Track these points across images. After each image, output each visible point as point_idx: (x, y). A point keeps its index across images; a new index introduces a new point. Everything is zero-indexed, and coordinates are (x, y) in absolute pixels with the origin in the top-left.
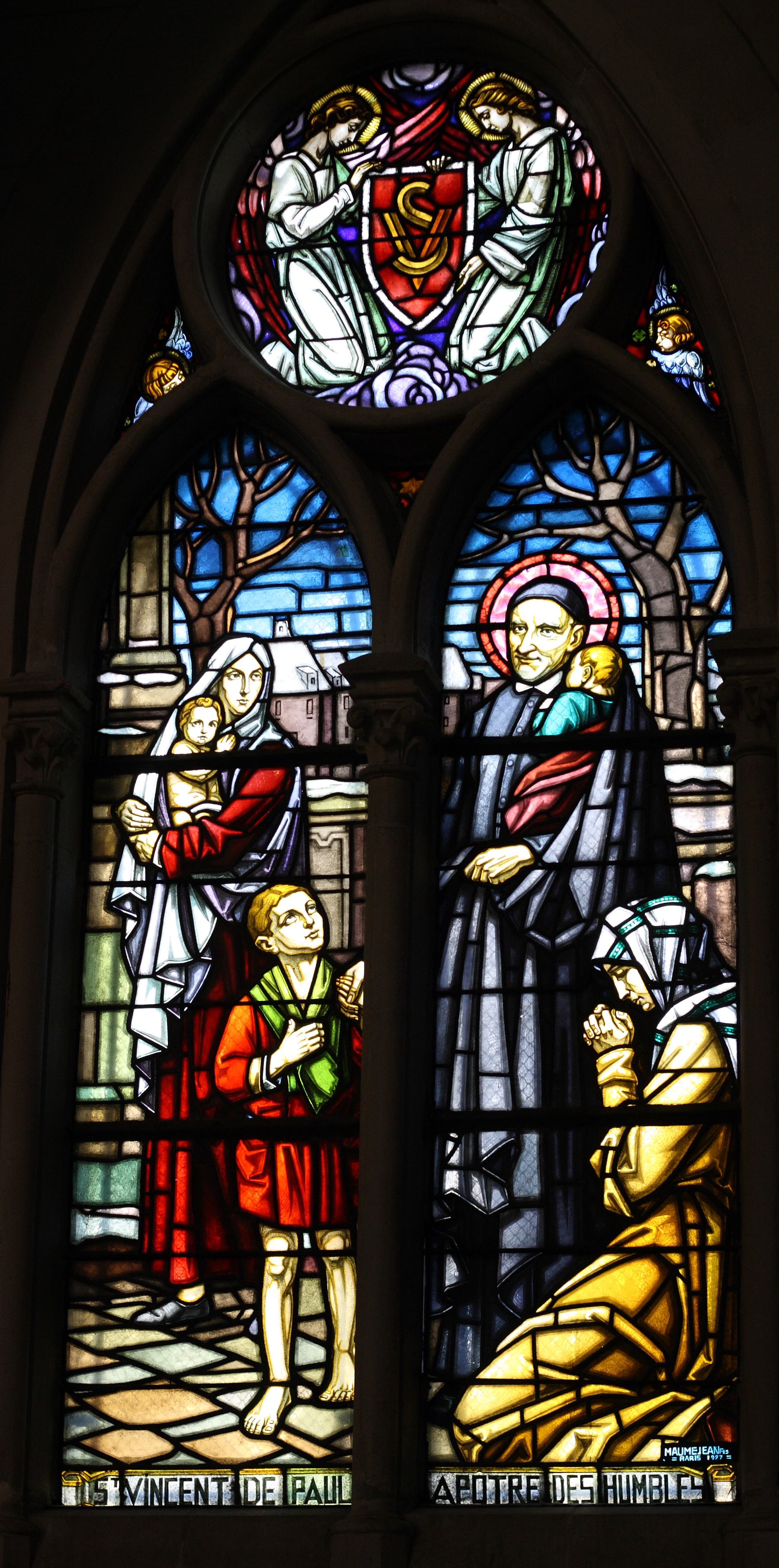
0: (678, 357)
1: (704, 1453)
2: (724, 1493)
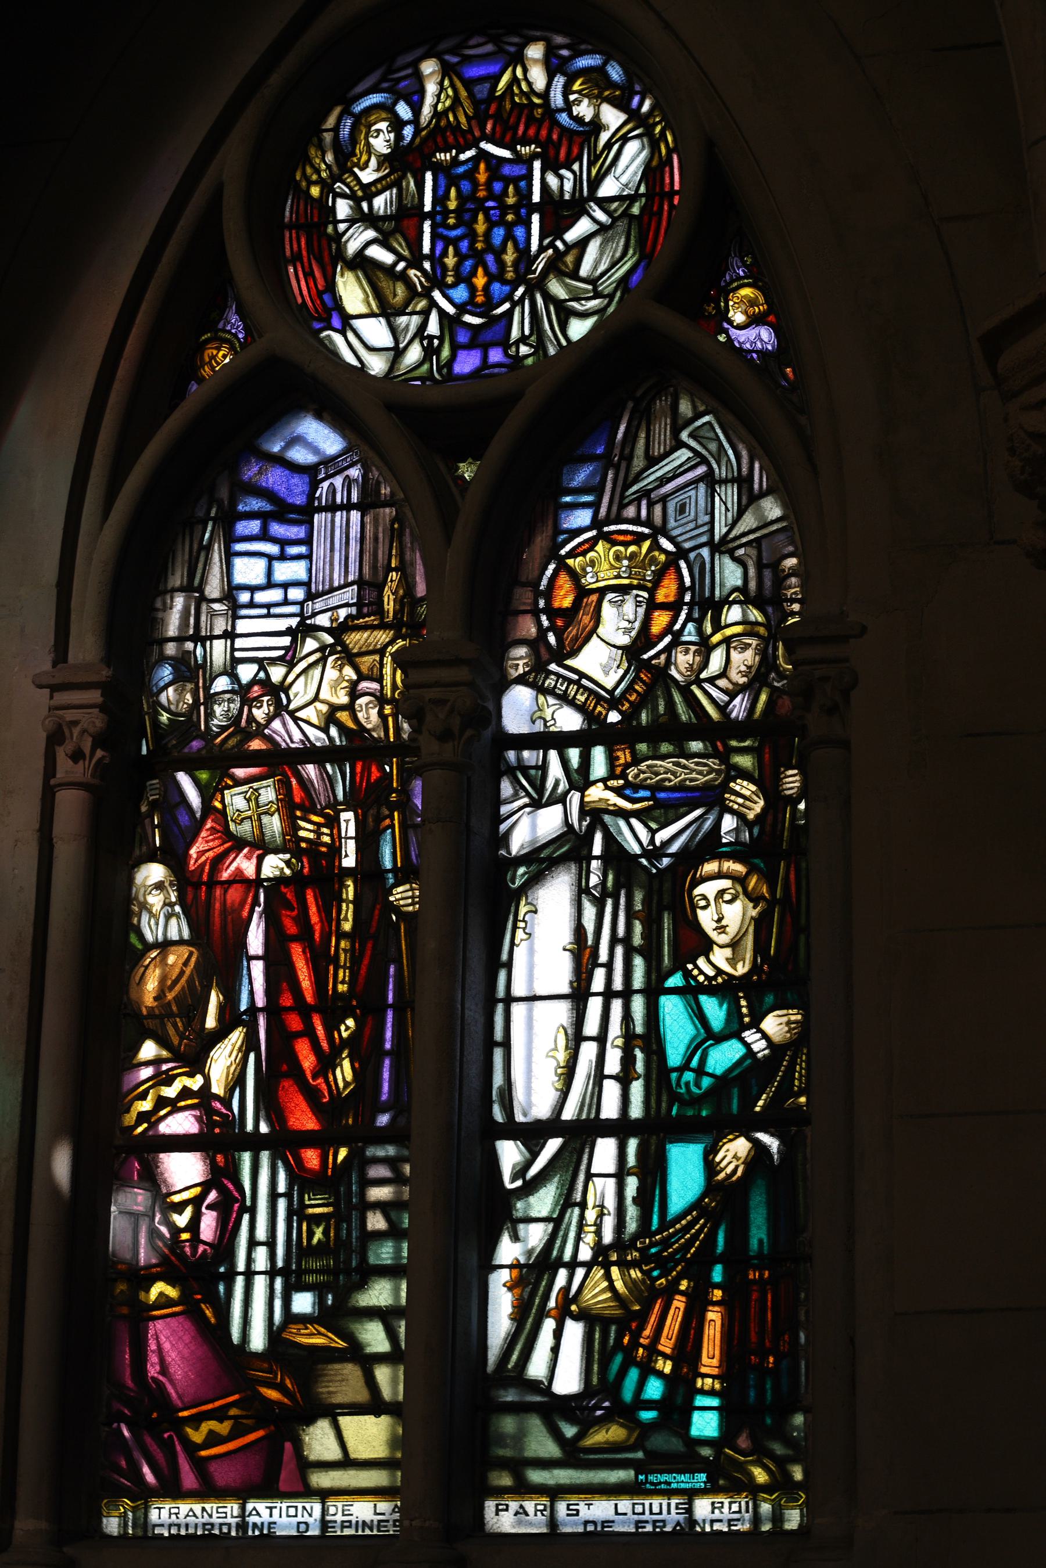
0: (751, 333)
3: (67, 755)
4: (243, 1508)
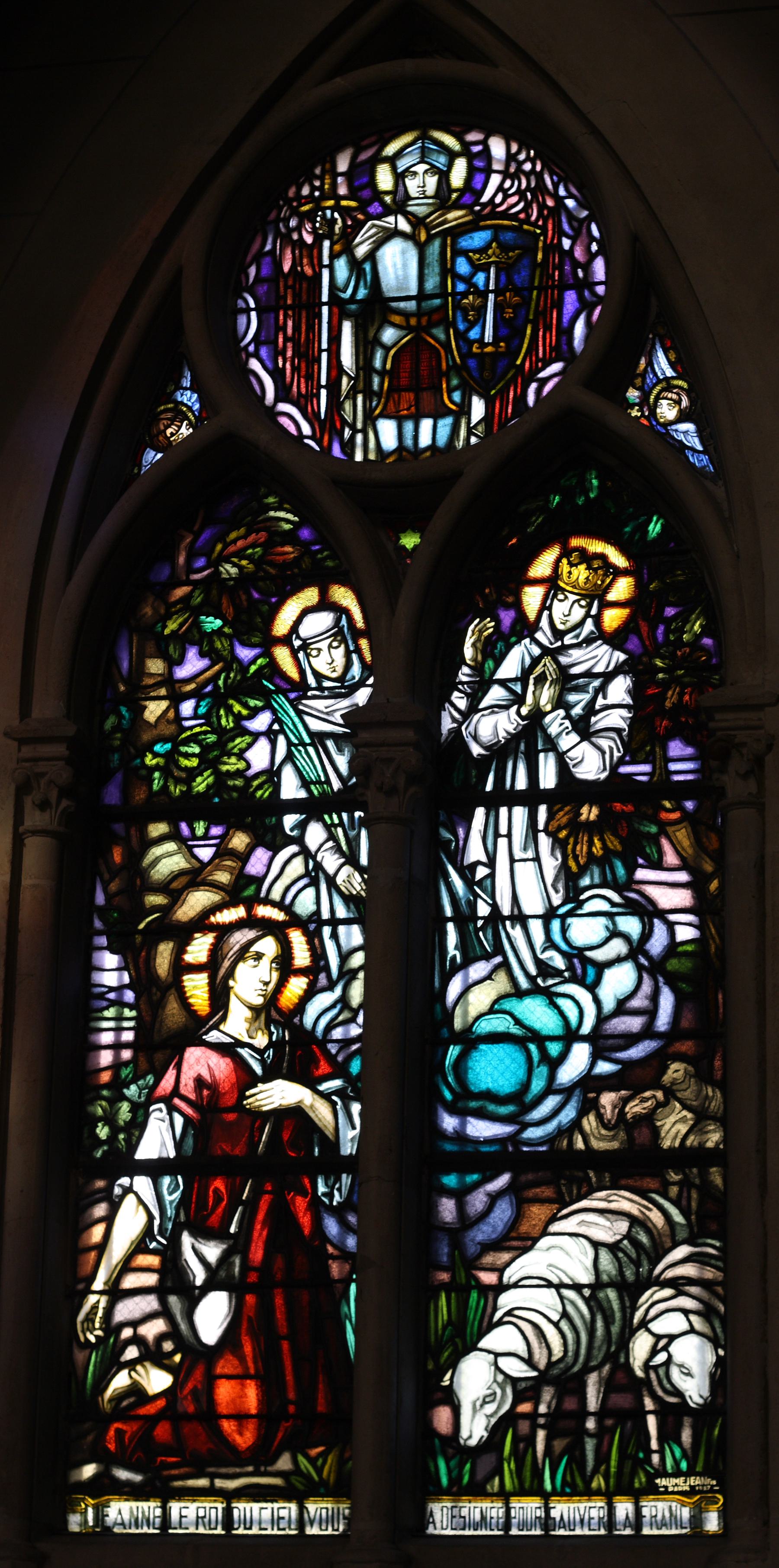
1: (692, 1484)
2: (712, 1523)
3: (33, 803)
4: (302, 1509)
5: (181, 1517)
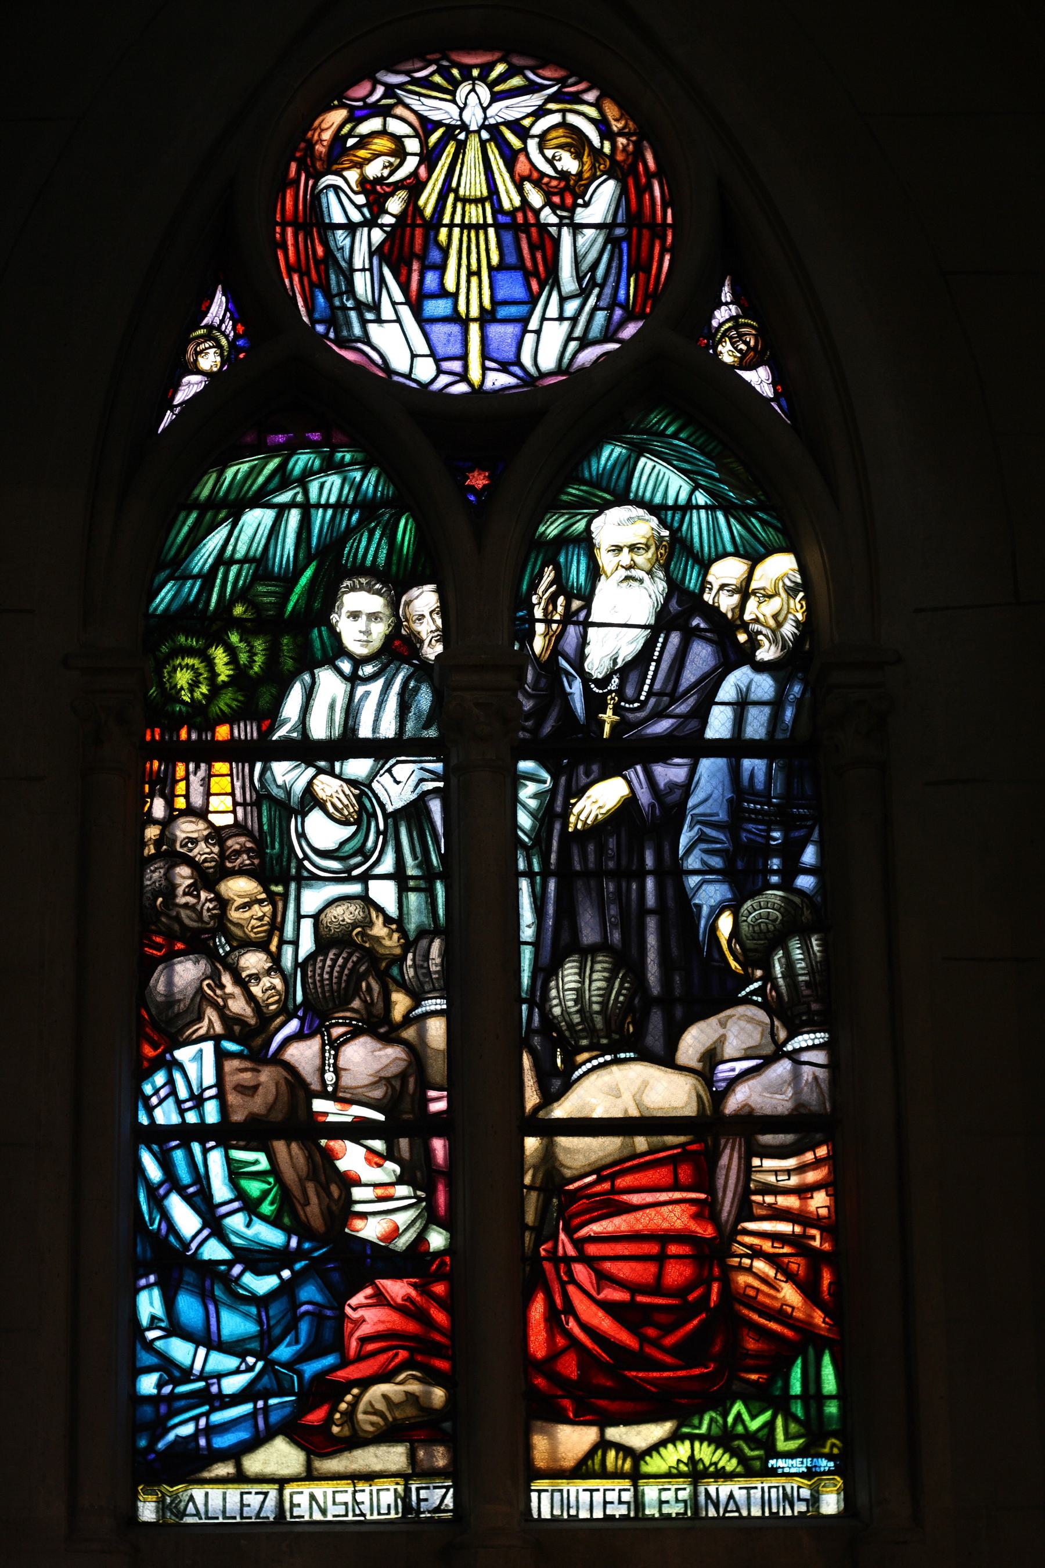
1: (809, 1465)
2: (830, 1504)
5: (242, 1505)
